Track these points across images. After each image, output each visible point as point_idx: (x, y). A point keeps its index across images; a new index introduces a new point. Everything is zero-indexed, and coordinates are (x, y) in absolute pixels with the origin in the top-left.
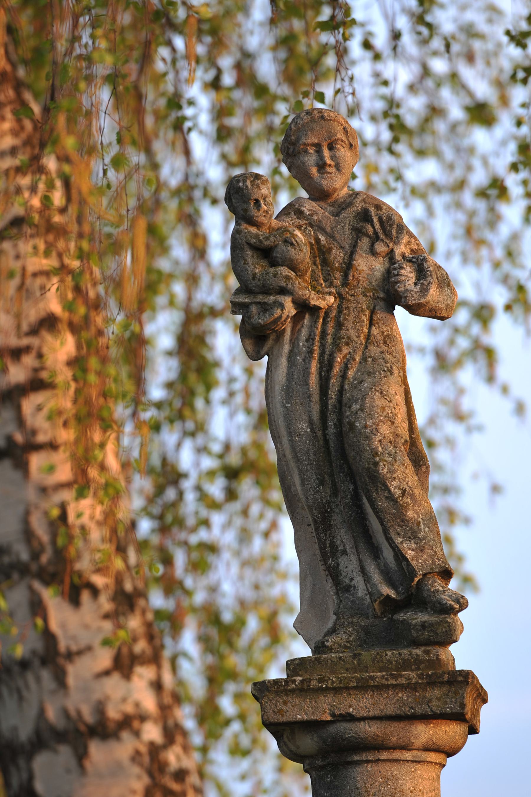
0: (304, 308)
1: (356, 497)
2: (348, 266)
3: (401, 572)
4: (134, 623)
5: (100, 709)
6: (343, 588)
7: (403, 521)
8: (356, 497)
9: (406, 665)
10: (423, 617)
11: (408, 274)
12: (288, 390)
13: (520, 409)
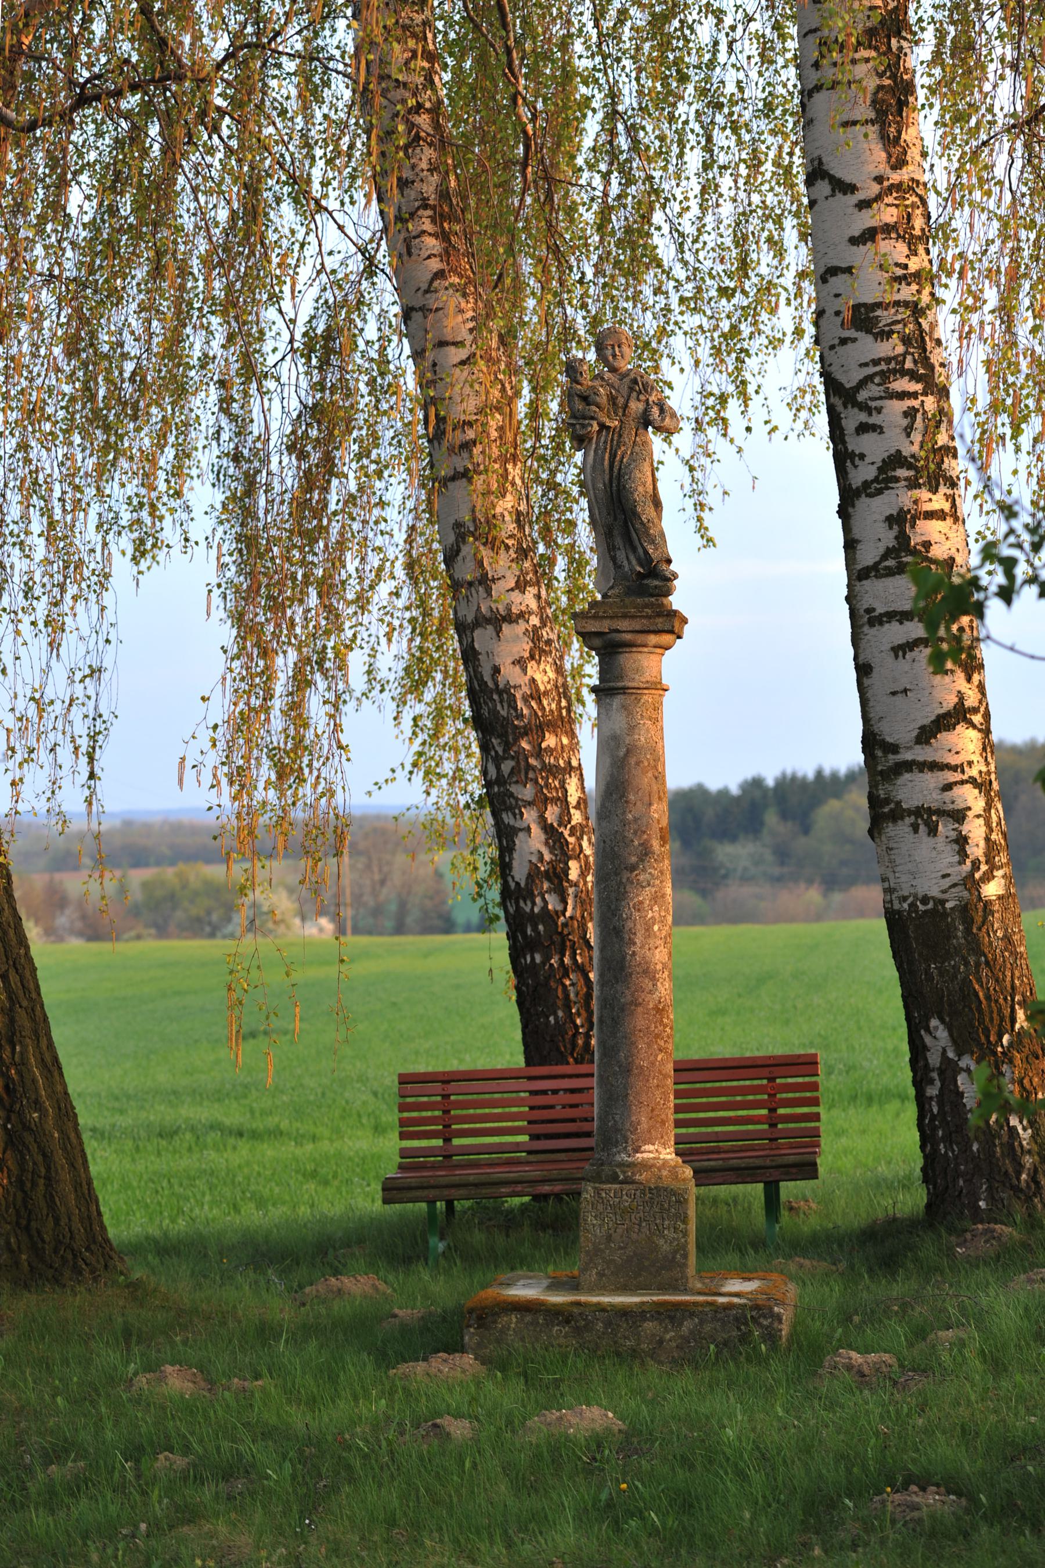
0: (603, 426)
1: (625, 522)
2: (626, 406)
3: (646, 560)
4: (527, 564)
5: (508, 608)
6: (618, 567)
7: (648, 535)
8: (625, 522)
9: (646, 606)
10: (656, 583)
11: (655, 411)
12: (594, 467)
13: (740, 450)
